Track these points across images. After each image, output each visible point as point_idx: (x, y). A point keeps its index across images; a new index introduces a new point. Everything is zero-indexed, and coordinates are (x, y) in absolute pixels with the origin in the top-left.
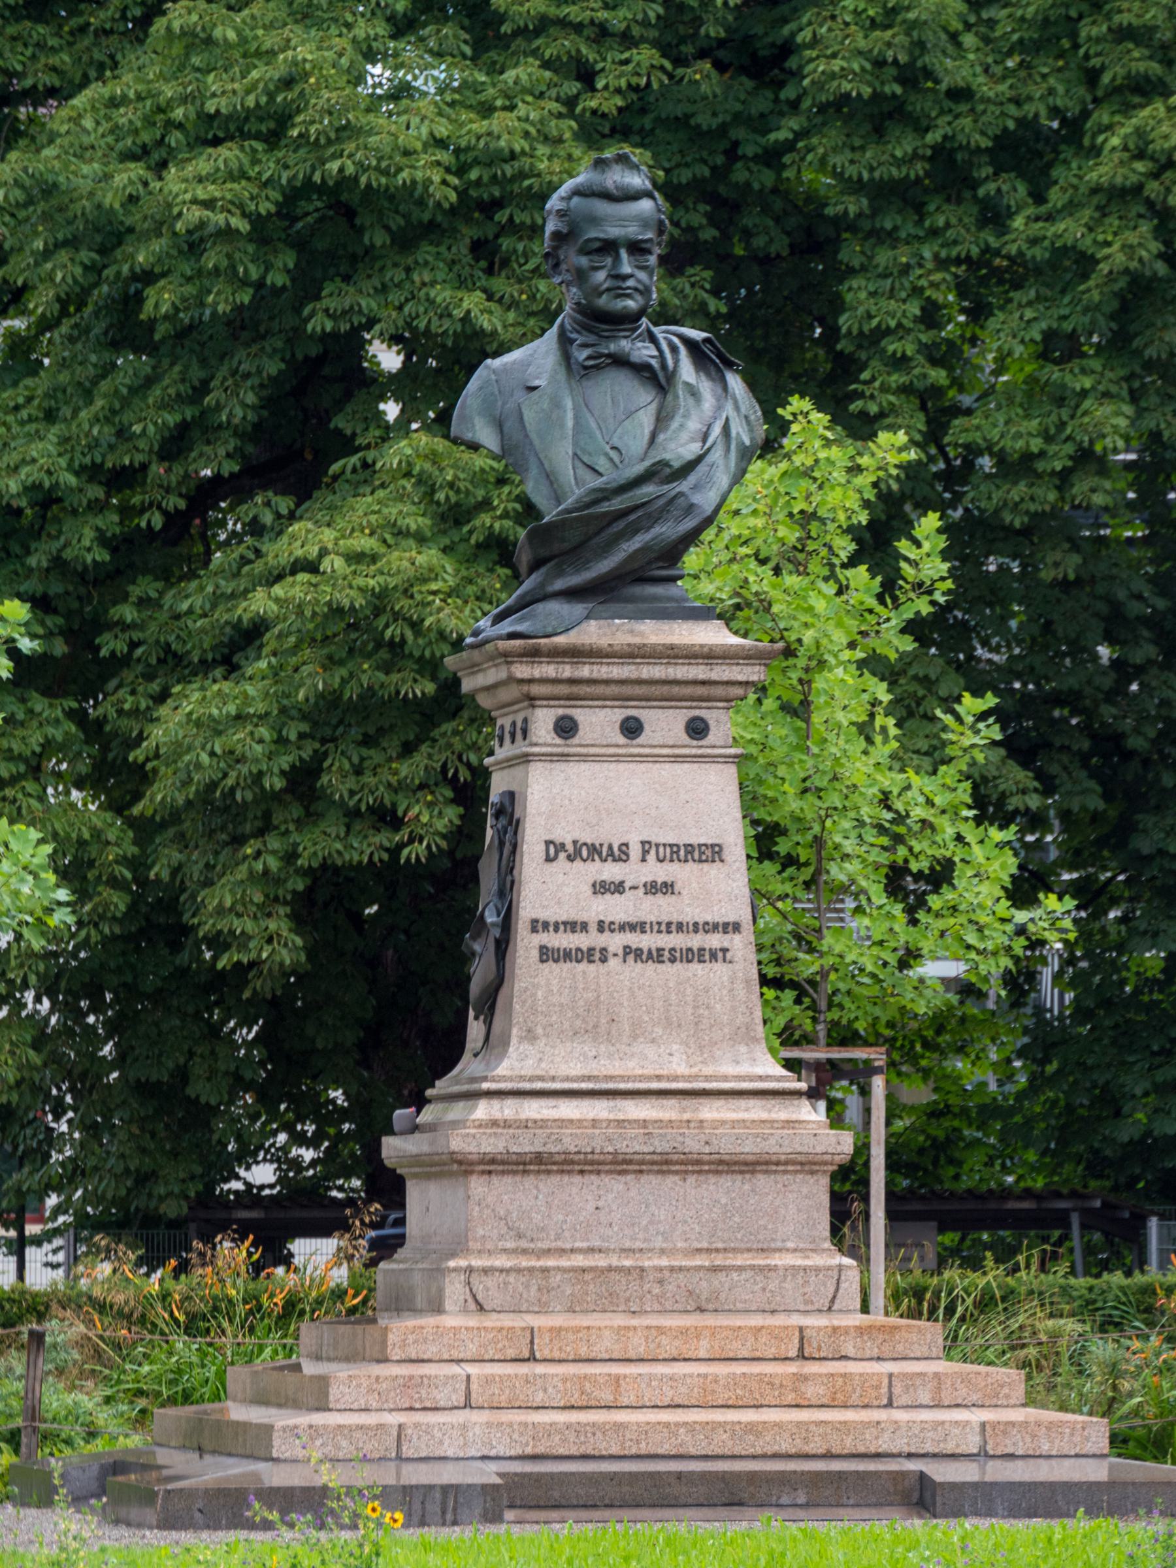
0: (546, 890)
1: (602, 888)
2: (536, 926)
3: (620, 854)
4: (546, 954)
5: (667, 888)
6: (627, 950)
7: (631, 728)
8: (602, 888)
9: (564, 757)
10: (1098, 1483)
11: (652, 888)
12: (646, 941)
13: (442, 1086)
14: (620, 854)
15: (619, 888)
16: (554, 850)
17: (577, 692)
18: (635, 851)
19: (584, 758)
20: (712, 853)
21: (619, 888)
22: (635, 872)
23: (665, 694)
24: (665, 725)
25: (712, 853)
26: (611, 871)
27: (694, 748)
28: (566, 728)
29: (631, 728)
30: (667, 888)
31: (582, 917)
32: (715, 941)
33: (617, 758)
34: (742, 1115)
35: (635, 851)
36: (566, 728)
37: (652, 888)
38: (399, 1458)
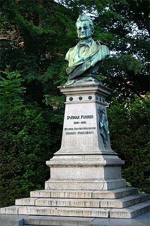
0: (67, 124)
1: (75, 123)
2: (66, 129)
3: (77, 118)
4: (68, 133)
5: (85, 122)
6: (79, 132)
7: (81, 98)
8: (75, 123)
9: (70, 103)
10: (20, 198)
11: (82, 123)
12: (81, 131)
13: (57, 153)
14: (77, 118)
15: (78, 123)
16: (68, 118)
17: (72, 94)
18: (80, 117)
19: (73, 103)
20: (91, 117)
21: (78, 123)
22: (80, 120)
23: (85, 93)
24: (85, 98)
25: (91, 117)
26: (76, 120)
27: (90, 101)
28: (71, 99)
29: (81, 98)
30: (85, 122)
31: (72, 128)
32: (91, 130)
33: (78, 103)
34: (104, 91)
35: (80, 117)
36: (71, 99)
37: (82, 123)
38: (109, 217)
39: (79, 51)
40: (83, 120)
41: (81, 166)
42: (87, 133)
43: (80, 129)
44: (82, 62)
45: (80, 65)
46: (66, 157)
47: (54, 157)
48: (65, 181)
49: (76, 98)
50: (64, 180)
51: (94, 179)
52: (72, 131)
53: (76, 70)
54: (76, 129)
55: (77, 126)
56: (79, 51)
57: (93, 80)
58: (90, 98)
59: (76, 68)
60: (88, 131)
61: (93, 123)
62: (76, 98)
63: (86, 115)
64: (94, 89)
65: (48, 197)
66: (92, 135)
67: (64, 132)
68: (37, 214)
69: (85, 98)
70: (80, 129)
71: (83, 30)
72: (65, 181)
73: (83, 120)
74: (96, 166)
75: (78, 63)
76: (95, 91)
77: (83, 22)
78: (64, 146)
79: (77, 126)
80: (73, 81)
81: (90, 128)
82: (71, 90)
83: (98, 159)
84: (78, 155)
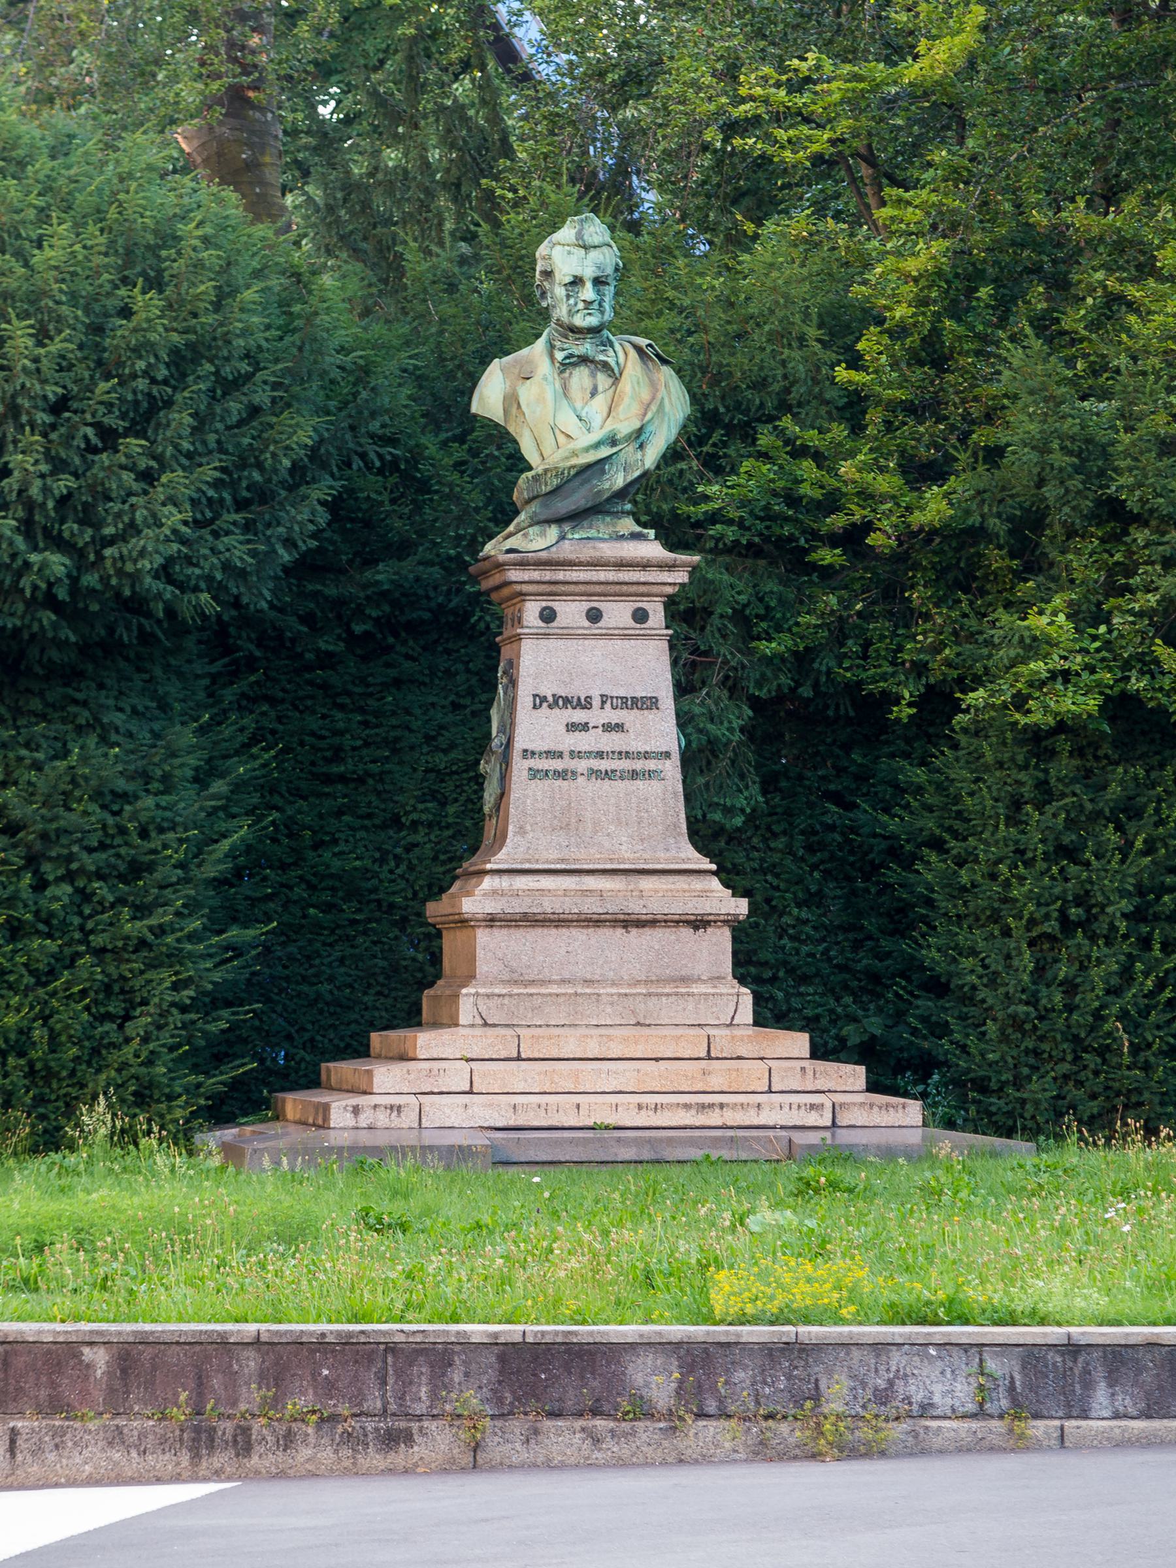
1: (572, 727)
2: (635, 769)
3: (585, 704)
4: (534, 774)
5: (619, 727)
7: (594, 616)
8: (572, 727)
9: (546, 635)
11: (608, 728)
12: (604, 765)
14: (585, 704)
15: (585, 727)
16: (539, 701)
17: (555, 590)
18: (596, 702)
20: (651, 703)
21: (585, 727)
22: (596, 716)
23: (617, 591)
25: (651, 703)
26: (579, 716)
28: (548, 616)
29: (594, 616)
30: (619, 727)
31: (560, 748)
32: (652, 765)
33: (585, 637)
35: (596, 702)
36: (548, 616)
37: (608, 728)
39: (565, 387)
40: (614, 716)
41: (629, 922)
42: (634, 775)
43: (600, 755)
44: (605, 452)
45: (589, 467)
46: (546, 882)
47: (488, 883)
48: (554, 989)
49: (571, 612)
50: (543, 982)
51: (685, 980)
52: (558, 765)
53: (576, 482)
54: (573, 754)
55: (582, 741)
56: (565, 387)
57: (651, 533)
58: (640, 616)
59: (578, 474)
60: (639, 765)
61: (660, 731)
62: (571, 612)
63: (622, 693)
64: (666, 577)
65: (503, 1055)
66: (655, 786)
67: (520, 767)
68: (512, 1123)
69: (618, 613)
70: (600, 755)
71: (588, 292)
72: (554, 989)
73: (614, 716)
74: (699, 923)
75: (587, 450)
76: (669, 590)
77: (593, 254)
78: (522, 831)
79: (582, 741)
80: (553, 532)
81: (646, 755)
82: (560, 576)
83: (704, 894)
84: (604, 872)
